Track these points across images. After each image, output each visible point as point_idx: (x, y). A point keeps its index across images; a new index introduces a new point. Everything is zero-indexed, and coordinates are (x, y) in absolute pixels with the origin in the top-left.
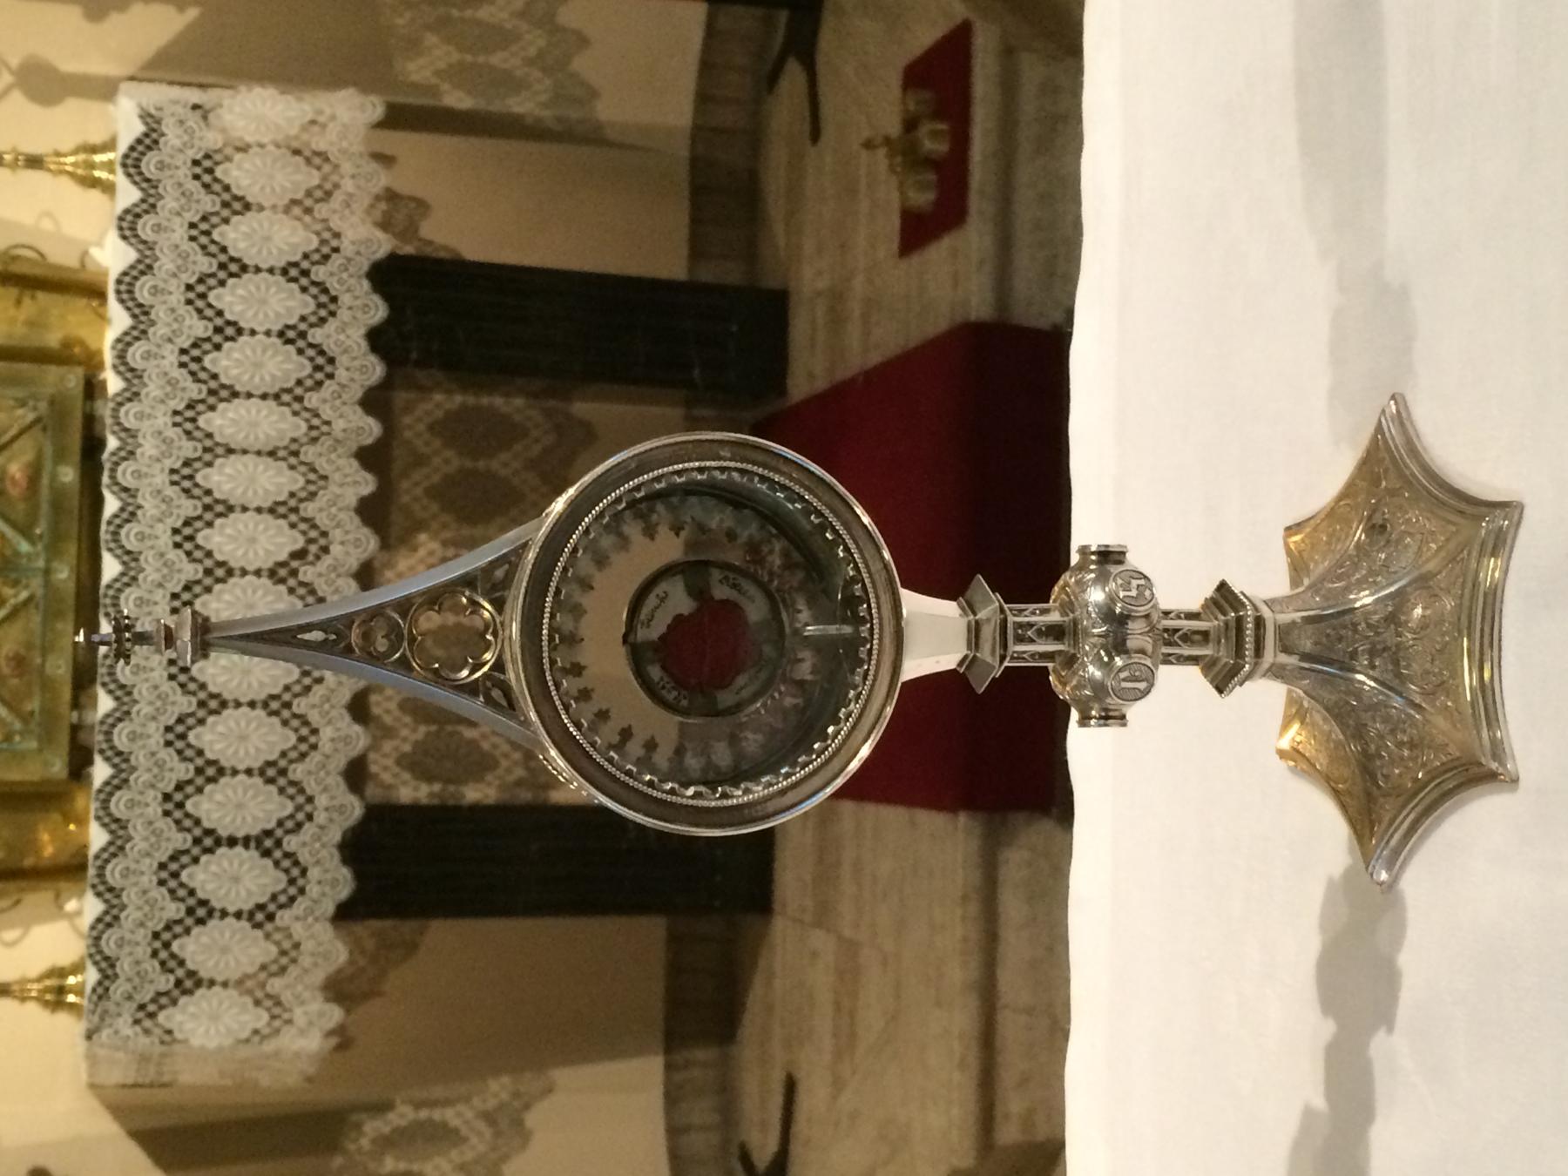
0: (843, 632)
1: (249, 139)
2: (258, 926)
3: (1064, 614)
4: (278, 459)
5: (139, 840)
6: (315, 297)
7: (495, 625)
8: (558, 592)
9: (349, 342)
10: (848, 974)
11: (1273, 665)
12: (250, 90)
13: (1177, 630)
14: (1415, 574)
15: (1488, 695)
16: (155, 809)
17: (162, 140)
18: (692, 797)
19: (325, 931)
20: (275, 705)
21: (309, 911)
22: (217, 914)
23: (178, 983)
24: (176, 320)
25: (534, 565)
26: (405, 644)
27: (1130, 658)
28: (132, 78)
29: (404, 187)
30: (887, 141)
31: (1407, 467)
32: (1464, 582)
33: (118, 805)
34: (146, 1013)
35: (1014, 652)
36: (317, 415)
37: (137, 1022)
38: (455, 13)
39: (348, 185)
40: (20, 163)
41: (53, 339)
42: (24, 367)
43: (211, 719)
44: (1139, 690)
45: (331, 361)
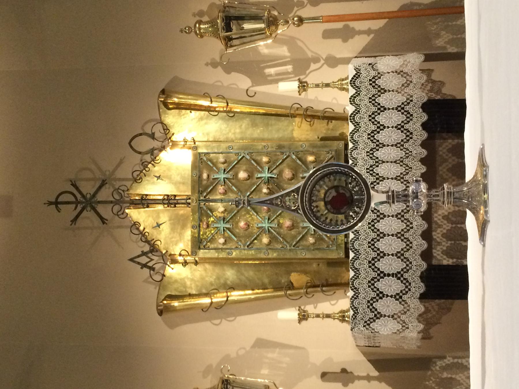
5: (363, 275)
6: (406, 115)
16: (366, 266)
19: (417, 302)
28: (356, 57)
34: (367, 324)
38: (450, 24)
45: (411, 133)
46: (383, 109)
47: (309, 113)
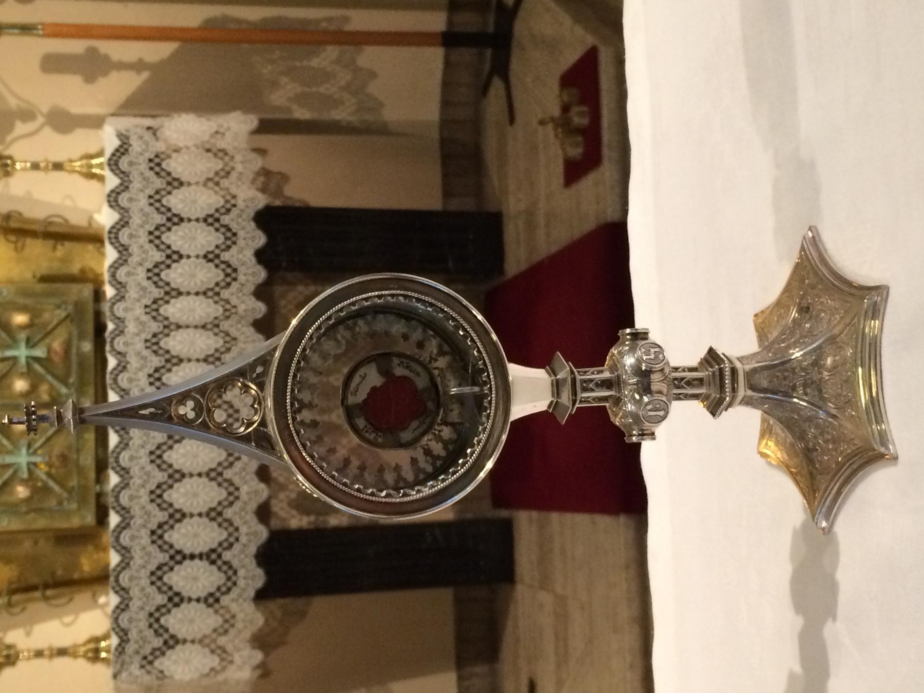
0: (473, 391)
1: (181, 144)
2: (210, 606)
3: (612, 372)
4: (208, 330)
5: (138, 559)
7: (259, 398)
8: (295, 376)
9: (245, 259)
10: (562, 617)
11: (745, 397)
12: (180, 117)
13: (682, 379)
14: (829, 335)
15: (875, 403)
17: (130, 149)
18: (385, 497)
20: (213, 474)
21: (240, 596)
22: (186, 600)
23: (166, 643)
24: (144, 252)
25: (279, 360)
26: (205, 413)
27: (653, 396)
28: (113, 115)
29: (274, 168)
30: (553, 120)
31: (821, 270)
32: (857, 336)
33: (125, 539)
34: (148, 661)
35: (581, 398)
37: (142, 667)
38: (298, 64)
39: (239, 167)
40: (49, 168)
41: (75, 269)
42: (58, 285)
44: (659, 416)
45: (235, 270)
46: (176, 220)
47: (13, 224)
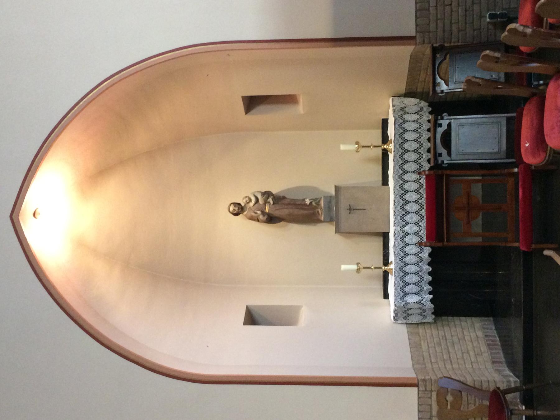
20: (416, 191)
21: (424, 160)
36: (421, 133)
43: (406, 164)
